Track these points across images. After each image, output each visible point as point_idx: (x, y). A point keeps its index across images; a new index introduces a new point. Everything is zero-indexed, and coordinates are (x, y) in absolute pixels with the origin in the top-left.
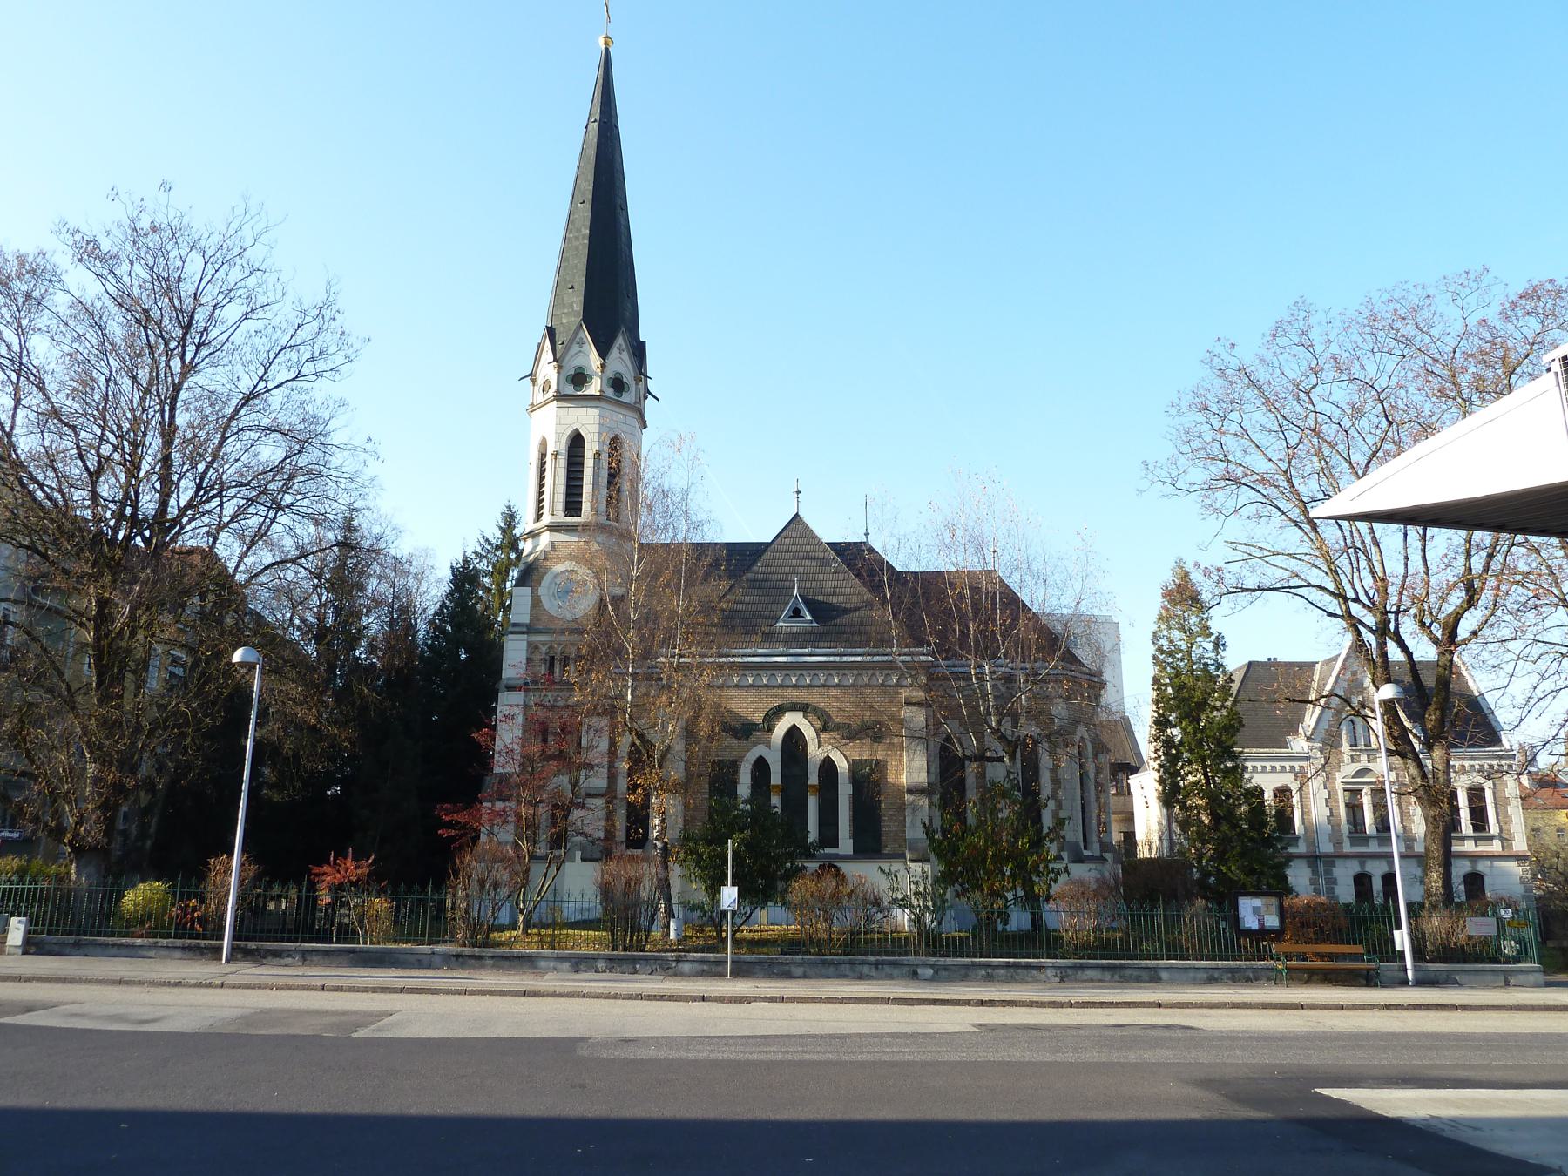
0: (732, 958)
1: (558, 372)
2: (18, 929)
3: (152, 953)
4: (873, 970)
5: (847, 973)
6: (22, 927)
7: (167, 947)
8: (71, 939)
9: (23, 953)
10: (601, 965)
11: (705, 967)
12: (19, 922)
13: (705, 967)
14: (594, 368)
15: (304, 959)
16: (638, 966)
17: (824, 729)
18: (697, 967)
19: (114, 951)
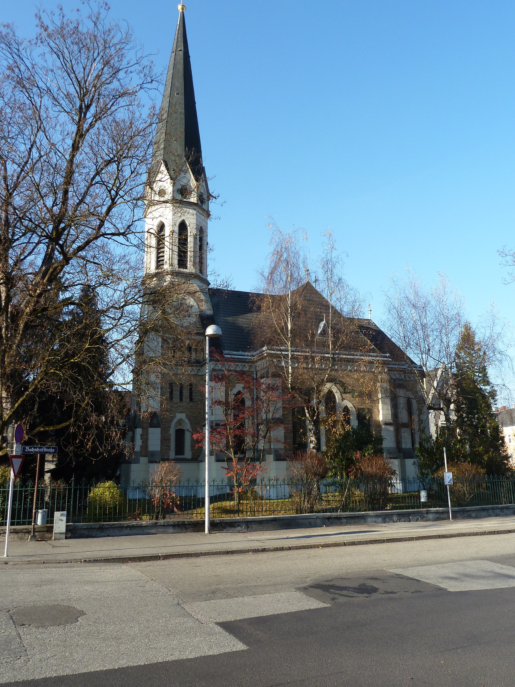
0: (451, 510)
1: (173, 186)
2: (62, 520)
3: (154, 531)
4: (500, 512)
5: (492, 514)
6: (64, 518)
7: (164, 525)
8: (97, 524)
9: (66, 538)
10: (395, 518)
11: (438, 516)
12: (62, 515)
13: (438, 516)
14: (193, 187)
15: (248, 527)
16: (411, 517)
17: (345, 393)
18: (436, 516)
19: (128, 531)
